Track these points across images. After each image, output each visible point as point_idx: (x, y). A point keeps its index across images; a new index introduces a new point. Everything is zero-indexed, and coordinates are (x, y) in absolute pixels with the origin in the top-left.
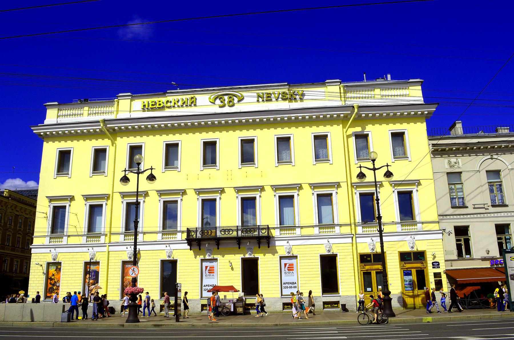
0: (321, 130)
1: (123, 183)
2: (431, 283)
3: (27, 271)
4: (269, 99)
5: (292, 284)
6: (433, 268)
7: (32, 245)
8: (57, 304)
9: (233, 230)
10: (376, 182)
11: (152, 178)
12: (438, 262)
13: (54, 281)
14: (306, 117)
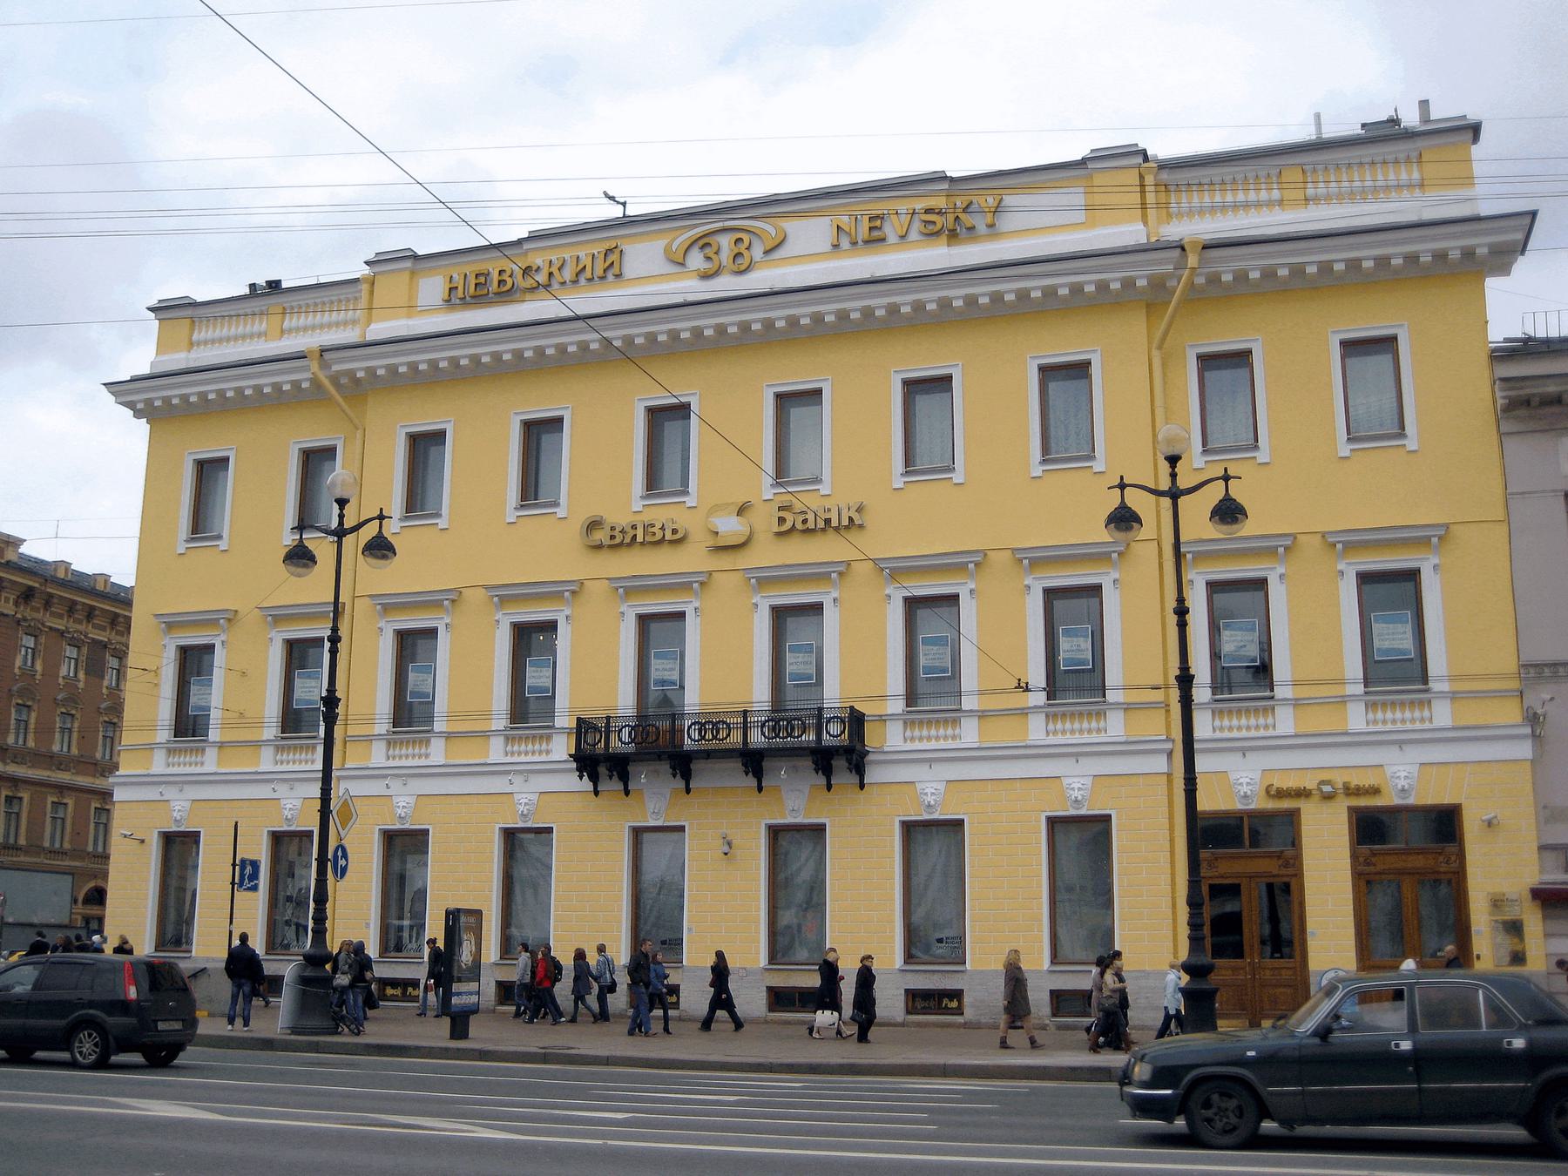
1: (293, 569)
3: (1177, 857)
4: (876, 234)
11: (380, 548)
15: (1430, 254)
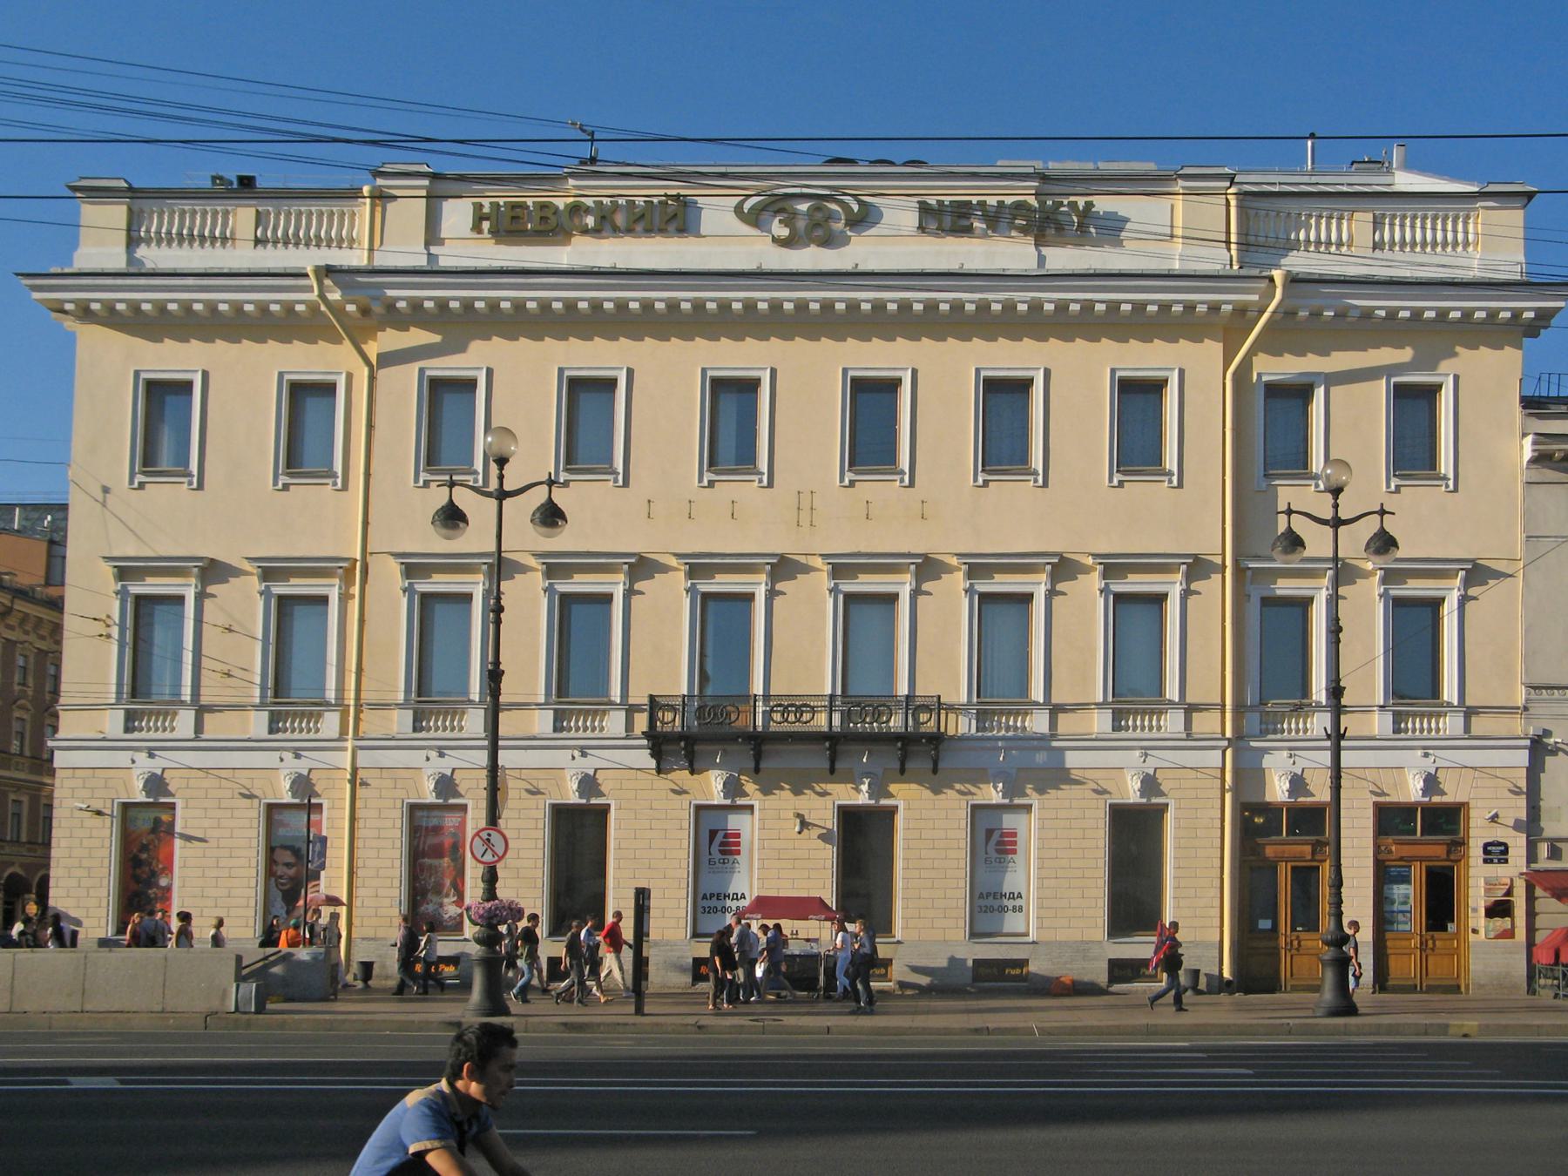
0: (1142, 358)
1: (444, 531)
2: (1475, 910)
5: (1009, 898)
6: (1485, 861)
7: (57, 736)
8: (74, 952)
9: (813, 707)
10: (1336, 559)
12: (1505, 845)
13: (150, 869)
14: (1097, 305)
15: (1206, 306)
